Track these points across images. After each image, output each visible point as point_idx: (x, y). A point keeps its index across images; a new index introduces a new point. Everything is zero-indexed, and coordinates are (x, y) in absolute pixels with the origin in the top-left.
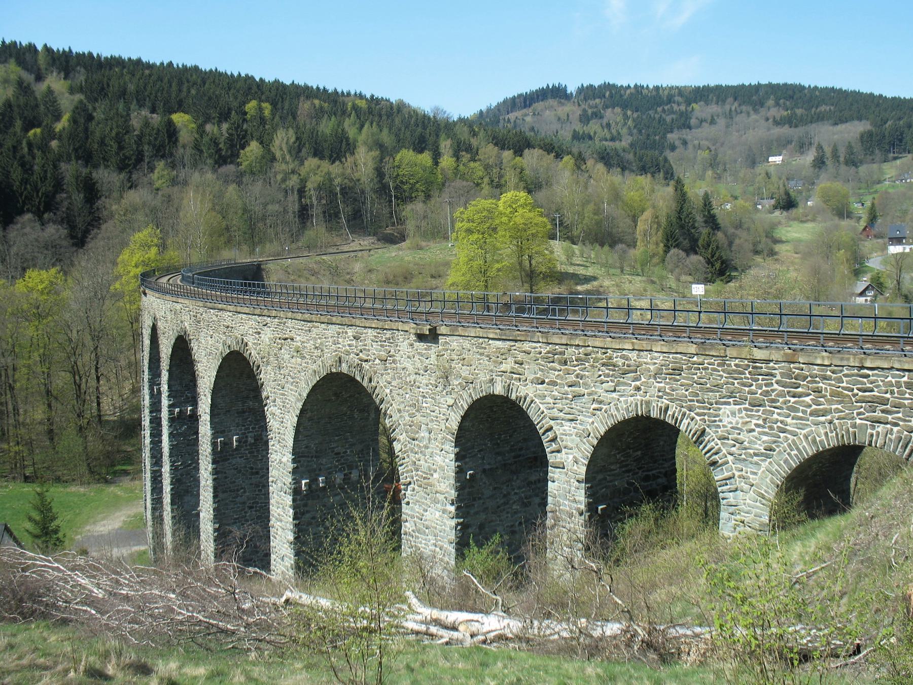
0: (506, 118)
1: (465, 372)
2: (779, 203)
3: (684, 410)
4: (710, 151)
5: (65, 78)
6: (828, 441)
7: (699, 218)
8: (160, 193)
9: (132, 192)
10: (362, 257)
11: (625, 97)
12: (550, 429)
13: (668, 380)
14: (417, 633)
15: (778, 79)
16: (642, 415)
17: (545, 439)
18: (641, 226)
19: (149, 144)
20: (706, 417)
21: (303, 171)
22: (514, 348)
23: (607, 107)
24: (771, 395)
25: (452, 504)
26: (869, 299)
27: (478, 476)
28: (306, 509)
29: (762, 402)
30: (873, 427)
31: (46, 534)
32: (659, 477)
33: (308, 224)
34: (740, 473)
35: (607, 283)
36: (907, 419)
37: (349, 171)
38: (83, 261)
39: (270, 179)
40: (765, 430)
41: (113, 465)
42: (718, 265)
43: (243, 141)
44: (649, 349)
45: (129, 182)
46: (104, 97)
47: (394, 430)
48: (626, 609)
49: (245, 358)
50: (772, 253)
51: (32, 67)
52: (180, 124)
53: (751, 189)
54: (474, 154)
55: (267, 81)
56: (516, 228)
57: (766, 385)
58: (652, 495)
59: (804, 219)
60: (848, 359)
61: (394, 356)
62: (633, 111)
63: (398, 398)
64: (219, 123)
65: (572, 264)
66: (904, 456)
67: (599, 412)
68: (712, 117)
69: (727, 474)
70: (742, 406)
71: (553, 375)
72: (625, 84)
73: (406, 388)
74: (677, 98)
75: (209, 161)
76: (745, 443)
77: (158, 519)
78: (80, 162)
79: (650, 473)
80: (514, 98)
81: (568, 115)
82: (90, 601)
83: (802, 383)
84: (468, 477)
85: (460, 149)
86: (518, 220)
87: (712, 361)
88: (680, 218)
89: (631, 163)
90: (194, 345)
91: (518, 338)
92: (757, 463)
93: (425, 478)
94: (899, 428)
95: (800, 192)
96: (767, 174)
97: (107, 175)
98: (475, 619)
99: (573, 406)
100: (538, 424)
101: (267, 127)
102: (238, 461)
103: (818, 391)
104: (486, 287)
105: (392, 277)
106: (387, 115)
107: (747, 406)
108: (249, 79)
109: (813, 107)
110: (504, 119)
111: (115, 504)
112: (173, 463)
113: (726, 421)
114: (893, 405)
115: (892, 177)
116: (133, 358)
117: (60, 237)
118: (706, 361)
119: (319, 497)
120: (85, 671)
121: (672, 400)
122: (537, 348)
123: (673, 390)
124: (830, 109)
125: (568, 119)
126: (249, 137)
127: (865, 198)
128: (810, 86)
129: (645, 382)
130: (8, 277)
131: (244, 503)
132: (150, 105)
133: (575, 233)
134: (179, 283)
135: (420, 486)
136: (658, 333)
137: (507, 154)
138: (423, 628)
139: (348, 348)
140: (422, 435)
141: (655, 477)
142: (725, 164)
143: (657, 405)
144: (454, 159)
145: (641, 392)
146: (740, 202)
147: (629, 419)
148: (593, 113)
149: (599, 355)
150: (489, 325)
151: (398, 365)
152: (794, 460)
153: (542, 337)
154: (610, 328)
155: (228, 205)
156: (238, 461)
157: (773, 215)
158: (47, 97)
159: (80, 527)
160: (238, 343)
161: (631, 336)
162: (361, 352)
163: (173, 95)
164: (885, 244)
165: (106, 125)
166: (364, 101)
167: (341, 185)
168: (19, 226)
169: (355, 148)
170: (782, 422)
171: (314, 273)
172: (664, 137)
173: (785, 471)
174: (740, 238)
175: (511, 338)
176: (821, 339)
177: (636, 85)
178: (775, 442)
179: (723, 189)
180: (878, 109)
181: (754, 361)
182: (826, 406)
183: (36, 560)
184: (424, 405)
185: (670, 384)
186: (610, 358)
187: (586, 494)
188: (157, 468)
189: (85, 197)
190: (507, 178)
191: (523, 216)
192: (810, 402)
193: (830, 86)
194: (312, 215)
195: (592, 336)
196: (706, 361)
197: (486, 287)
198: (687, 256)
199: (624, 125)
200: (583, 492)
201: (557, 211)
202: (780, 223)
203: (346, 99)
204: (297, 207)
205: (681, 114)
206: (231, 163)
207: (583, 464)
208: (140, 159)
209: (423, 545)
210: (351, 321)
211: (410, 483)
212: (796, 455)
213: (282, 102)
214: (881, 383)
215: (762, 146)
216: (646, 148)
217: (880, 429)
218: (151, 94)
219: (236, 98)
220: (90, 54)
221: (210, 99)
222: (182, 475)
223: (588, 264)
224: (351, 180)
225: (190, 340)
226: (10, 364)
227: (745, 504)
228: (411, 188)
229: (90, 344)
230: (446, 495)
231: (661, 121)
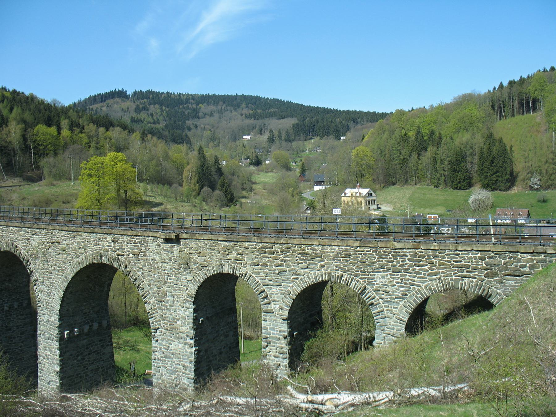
1: (201, 260)
2: (253, 162)
13: (342, 261)
22: (237, 245)
29: (400, 270)
34: (387, 308)
35: (169, 207)
40: (402, 285)
44: (330, 244)
50: (251, 190)
53: (235, 153)
54: (82, 129)
60: (449, 246)
62: (166, 107)
65: (147, 196)
67: (297, 280)
68: (211, 112)
69: (379, 309)
70: (388, 273)
71: (265, 261)
73: (155, 271)
76: (390, 292)
80: (95, 96)
81: (128, 108)
83: (422, 259)
84: (200, 322)
88: (203, 170)
91: (240, 240)
92: (397, 303)
93: (170, 325)
96: (243, 145)
98: (335, 397)
99: (279, 277)
103: (432, 263)
105: (38, 203)
107: (391, 273)
109: (266, 109)
110: (90, 108)
113: (378, 281)
118: (365, 250)
119: (74, 341)
121: (345, 272)
122: (253, 245)
123: (345, 266)
125: (128, 110)
128: (264, 97)
129: (327, 262)
133: (144, 177)
137: (102, 130)
140: (168, 299)
142: (219, 139)
144: (70, 131)
145: (325, 268)
147: (317, 283)
152: (419, 300)
153: (257, 239)
169: (8, 121)
170: (411, 280)
172: (184, 122)
175: (235, 240)
177: (167, 93)
178: (408, 291)
181: (395, 249)
182: (437, 271)
184: (169, 281)
185: (343, 263)
186: (304, 250)
192: (428, 269)
196: (365, 250)
202: (254, 173)
205: (194, 110)
207: (286, 310)
209: (169, 365)
211: (159, 328)
212: (420, 297)
214: (466, 258)
217: (466, 281)
223: (156, 196)
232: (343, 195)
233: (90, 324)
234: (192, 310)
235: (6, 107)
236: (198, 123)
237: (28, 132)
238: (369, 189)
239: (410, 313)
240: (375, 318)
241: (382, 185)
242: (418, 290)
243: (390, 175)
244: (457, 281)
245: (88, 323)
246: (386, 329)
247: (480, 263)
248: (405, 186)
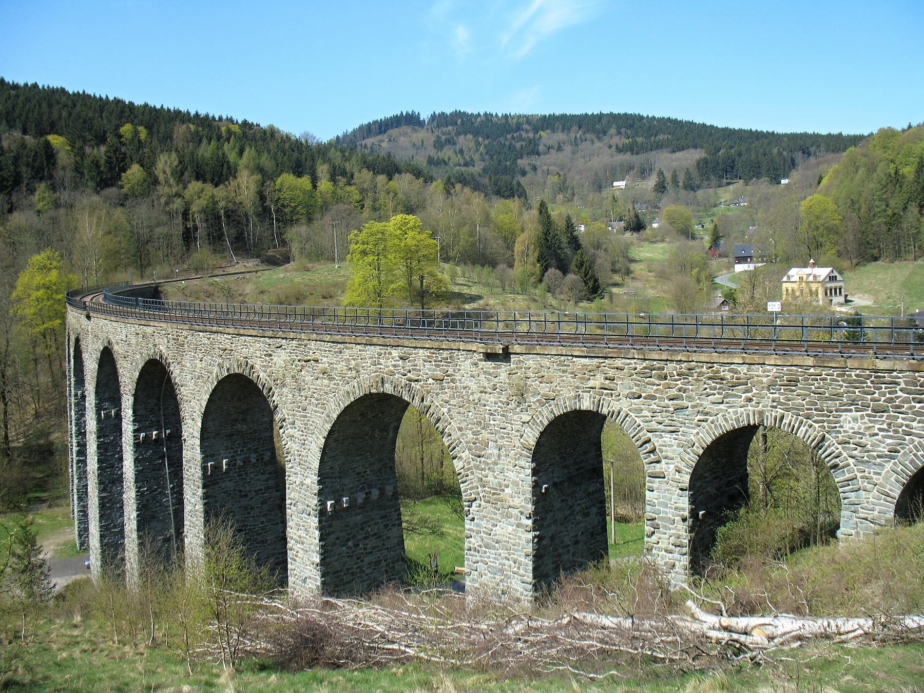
0: (363, 143)
1: (544, 389)
2: (630, 225)
4: (560, 176)
12: (648, 441)
13: (782, 391)
15: (619, 109)
19: (27, 165)
21: (187, 194)
22: (604, 364)
28: (331, 530)
29: (886, 409)
33: (192, 246)
34: (863, 474)
35: (491, 302)
40: (889, 433)
41: (26, 493)
43: (122, 164)
49: (251, 381)
50: (628, 272)
52: (58, 145)
55: (136, 104)
57: (890, 393)
59: (654, 240)
61: (452, 375)
68: (559, 144)
69: (847, 476)
70: (864, 413)
71: (651, 390)
72: (475, 113)
74: (526, 126)
75: (90, 184)
79: (730, 479)
81: (422, 142)
84: (543, 491)
87: (831, 372)
90: (175, 371)
91: (610, 355)
92: (880, 465)
93: (494, 494)
96: (614, 198)
99: (675, 418)
102: (229, 485)
107: (870, 412)
110: (361, 145)
112: (139, 491)
113: (847, 427)
118: (824, 373)
122: (631, 364)
124: (668, 139)
125: (422, 145)
126: (128, 160)
128: (648, 116)
132: (21, 126)
133: (451, 254)
137: (381, 178)
140: (490, 452)
142: (573, 189)
143: (771, 415)
144: (332, 183)
145: (753, 403)
148: (446, 140)
149: (704, 370)
151: (458, 384)
153: (638, 354)
156: (229, 485)
160: (240, 366)
166: (237, 127)
169: (236, 171)
170: (907, 426)
171: (209, 295)
172: (514, 162)
175: (600, 355)
184: (492, 422)
185: (785, 394)
186: (718, 372)
190: (381, 201)
200: (687, 499)
203: (220, 124)
205: (530, 141)
206: (112, 185)
208: (17, 182)
210: (397, 342)
211: (475, 500)
219: (110, 121)
221: (85, 122)
222: (148, 501)
223: (470, 284)
227: (868, 502)
232: (785, 279)
233: (367, 491)
234: (529, 471)
236: (538, 163)
238: (831, 269)
241: (855, 261)
243: (868, 243)
245: (363, 489)
248: (896, 262)
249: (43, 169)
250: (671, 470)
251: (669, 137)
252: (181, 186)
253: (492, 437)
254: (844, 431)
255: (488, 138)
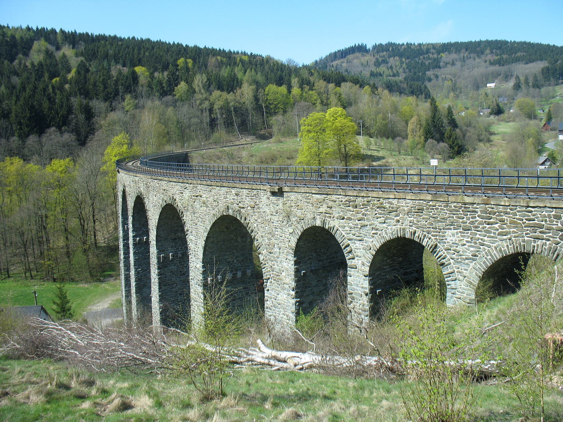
1: (299, 213)
2: (493, 111)
3: (424, 233)
5: (73, 48)
6: (509, 250)
7: (445, 121)
8: (129, 113)
9: (113, 113)
10: (247, 148)
11: (401, 51)
12: (348, 245)
13: (415, 216)
14: (263, 364)
16: (401, 237)
17: (345, 252)
18: (410, 127)
19: (122, 85)
20: (438, 237)
21: (212, 98)
22: (327, 198)
23: (390, 57)
24: (475, 224)
25: (293, 290)
26: (547, 167)
27: (308, 274)
29: (470, 228)
30: (535, 242)
31: (64, 311)
32: (413, 273)
33: (215, 129)
34: (458, 270)
35: (390, 160)
36: (555, 236)
37: (239, 98)
38: (84, 154)
39: (193, 103)
42: (456, 149)
44: (404, 198)
45: (111, 107)
46: (95, 58)
47: (259, 248)
48: (376, 349)
49: (175, 208)
50: (489, 141)
51: (54, 42)
53: (476, 103)
55: (190, 46)
56: (336, 129)
57: (472, 218)
58: (408, 283)
59: (508, 120)
60: (520, 202)
61: (258, 205)
63: (261, 229)
64: (163, 71)
66: (553, 259)
68: (453, 61)
69: (450, 271)
70: (458, 231)
71: (349, 214)
75: (157, 94)
77: (129, 302)
78: (82, 96)
79: (408, 271)
82: (76, 347)
83: (493, 216)
85: (303, 83)
86: (338, 124)
88: (434, 121)
89: (404, 89)
90: (146, 201)
91: (329, 193)
92: (467, 264)
93: (277, 275)
94: (550, 242)
95: (506, 104)
96: (486, 94)
97: (97, 104)
99: (361, 232)
100: (341, 243)
101: (190, 73)
102: (173, 268)
104: (320, 163)
105: (264, 159)
106: (260, 64)
107: (461, 230)
108: (179, 46)
111: (105, 293)
113: (449, 239)
114: (546, 228)
115: (561, 94)
116: (114, 209)
117: (71, 140)
118: (437, 204)
120: (56, 384)
121: (418, 228)
123: (418, 222)
126: (180, 79)
127: (545, 107)
128: (511, 41)
129: (402, 217)
130: (42, 164)
131: (177, 292)
133: (372, 131)
134: (139, 165)
135: (275, 280)
136: (394, 188)
137: (331, 86)
138: (266, 361)
139: (232, 200)
140: (275, 250)
141: (411, 273)
142: (461, 89)
145: (400, 223)
146: (470, 111)
150: (312, 185)
153: (343, 192)
154: (397, 187)
155: (168, 119)
156: (173, 268)
157: (490, 118)
158: (62, 59)
159: (85, 307)
161: (394, 190)
162: (240, 202)
163: (136, 56)
164: (557, 134)
165: (97, 75)
166: (247, 57)
167: (234, 106)
168: (48, 134)
169: (241, 84)
170: (481, 239)
171: (219, 158)
172: (424, 73)
173: (484, 268)
174: (470, 132)
175: (325, 193)
176: (505, 190)
177: (407, 44)
178: (478, 251)
179: (460, 104)
180: (552, 53)
183: (49, 325)
184: (276, 233)
185: (416, 218)
186: (382, 204)
187: (369, 283)
188: (128, 273)
189: (85, 117)
190: (331, 99)
191: (340, 122)
192: (498, 227)
193: (523, 40)
194: (218, 124)
195: (371, 191)
196: (437, 204)
197: (320, 163)
198: (438, 143)
199: (400, 67)
200: (368, 282)
201: (361, 118)
202: (493, 123)
203: (236, 56)
204: (208, 120)
205: (435, 60)
206: (170, 94)
207: (367, 266)
208: (117, 93)
211: (269, 278)
212: (490, 259)
213: (199, 58)
214: (539, 216)
215: (483, 78)
216: (414, 80)
217: (539, 243)
218: (122, 56)
219: (172, 57)
220: (87, 34)
221: (157, 58)
222: (141, 276)
223: (379, 150)
224: (240, 103)
225: (144, 198)
226: (44, 214)
227: (461, 288)
228: (275, 107)
229: (90, 202)
230: (290, 285)
231: (423, 64)
233: (234, 272)
234: (293, 262)
235: (241, 70)
236: (439, 74)
237: (260, 92)
239: (480, 277)
240: (446, 279)
242: (488, 250)
244: (529, 242)
246: (457, 292)
247: (555, 223)
249: (131, 86)
250: (359, 264)
251: (525, 54)
252: (208, 94)
253: (276, 242)
254: (448, 242)
255: (408, 59)
